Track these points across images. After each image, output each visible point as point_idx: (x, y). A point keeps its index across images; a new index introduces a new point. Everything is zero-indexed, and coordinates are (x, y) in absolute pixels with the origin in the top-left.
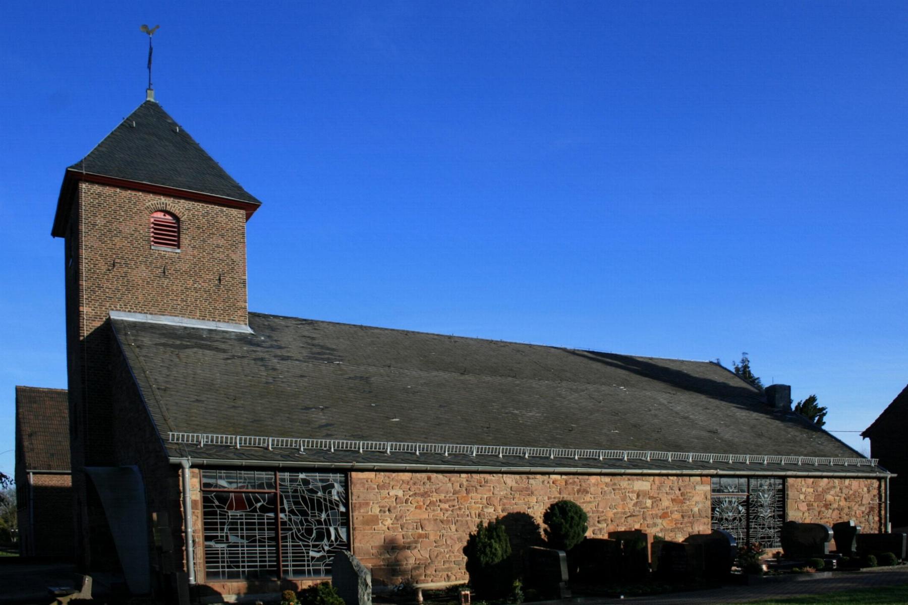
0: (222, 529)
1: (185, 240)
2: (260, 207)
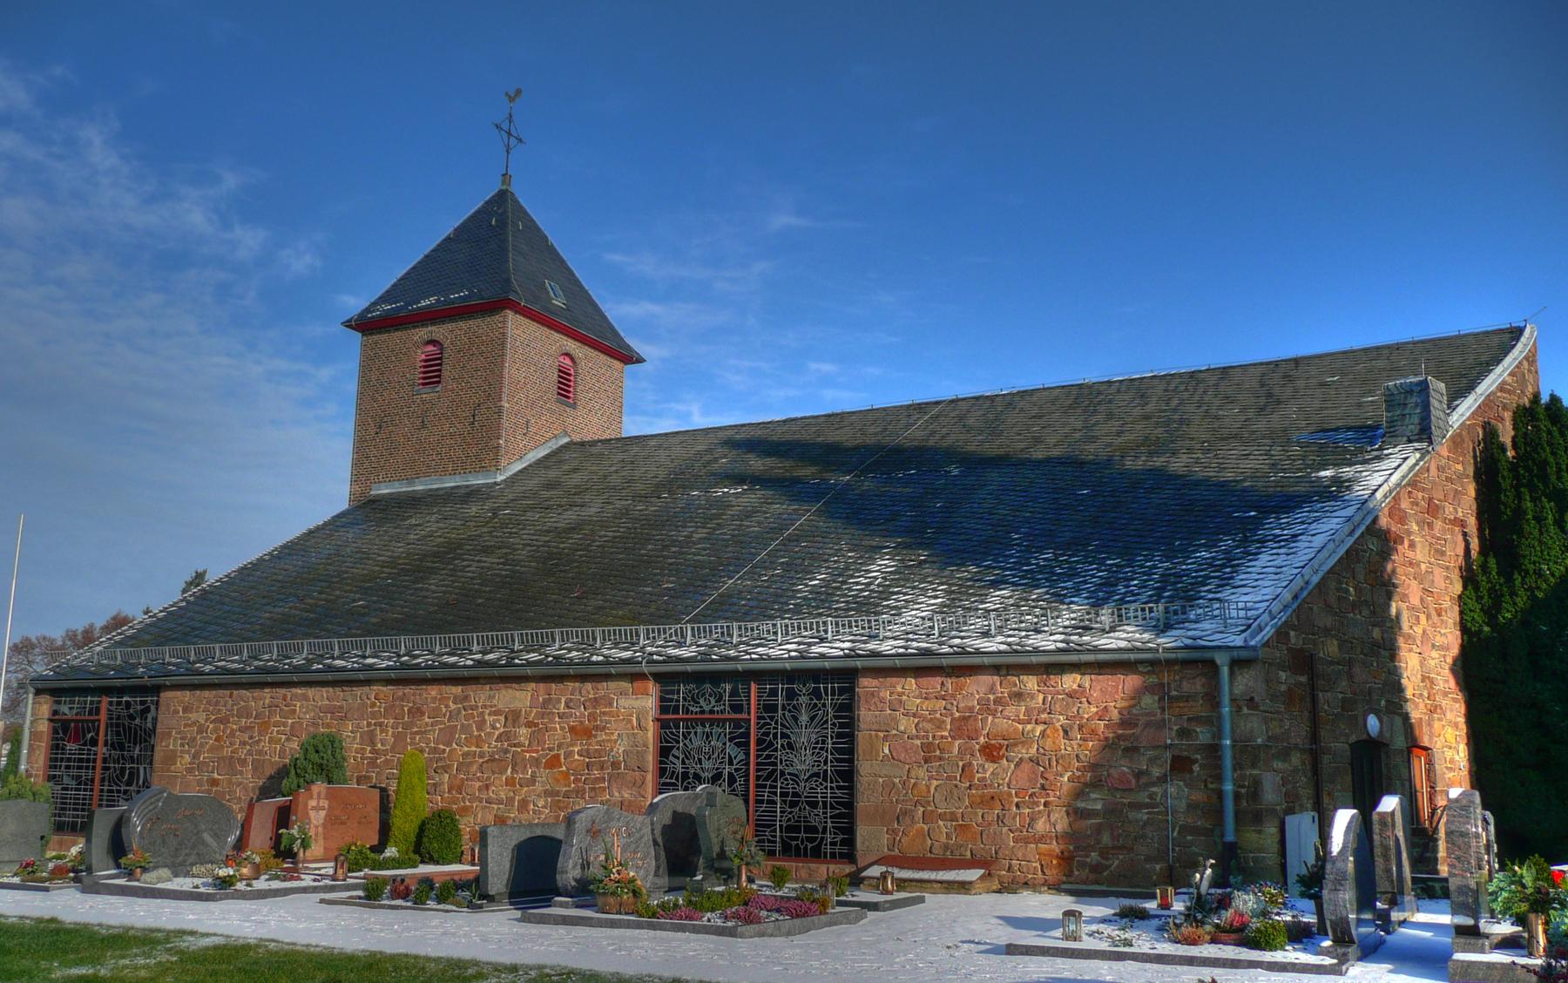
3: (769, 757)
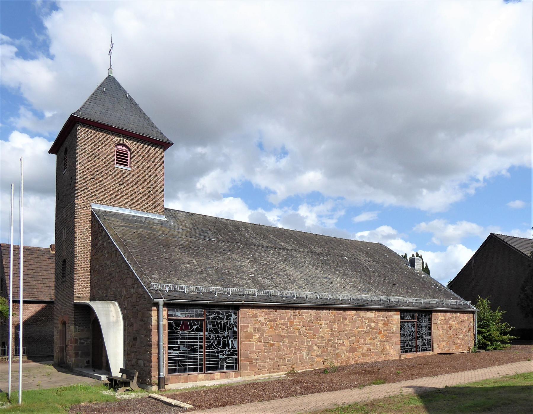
0: (177, 342)
3: (418, 330)
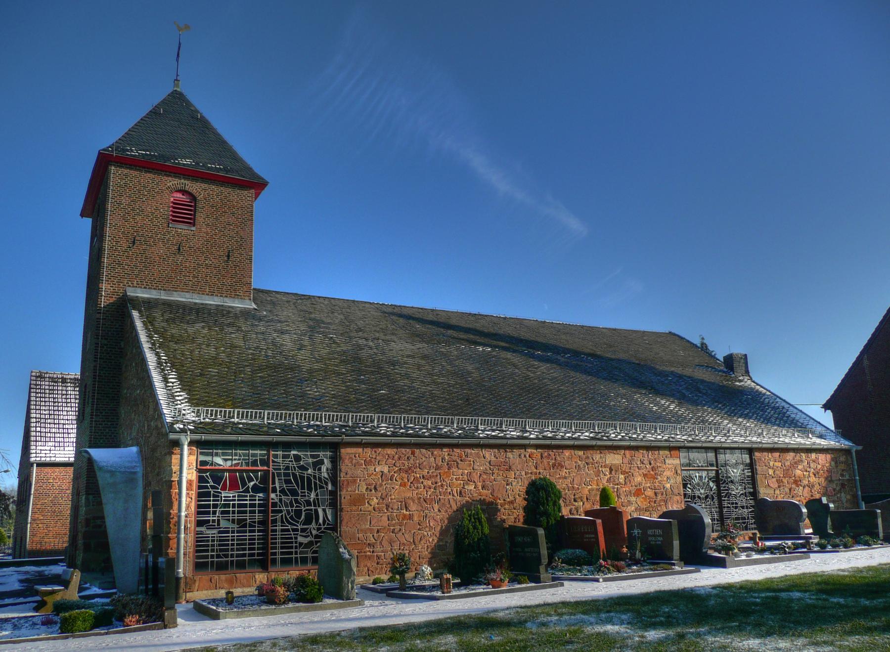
0: (214, 513)
1: (200, 217)
2: (267, 187)
